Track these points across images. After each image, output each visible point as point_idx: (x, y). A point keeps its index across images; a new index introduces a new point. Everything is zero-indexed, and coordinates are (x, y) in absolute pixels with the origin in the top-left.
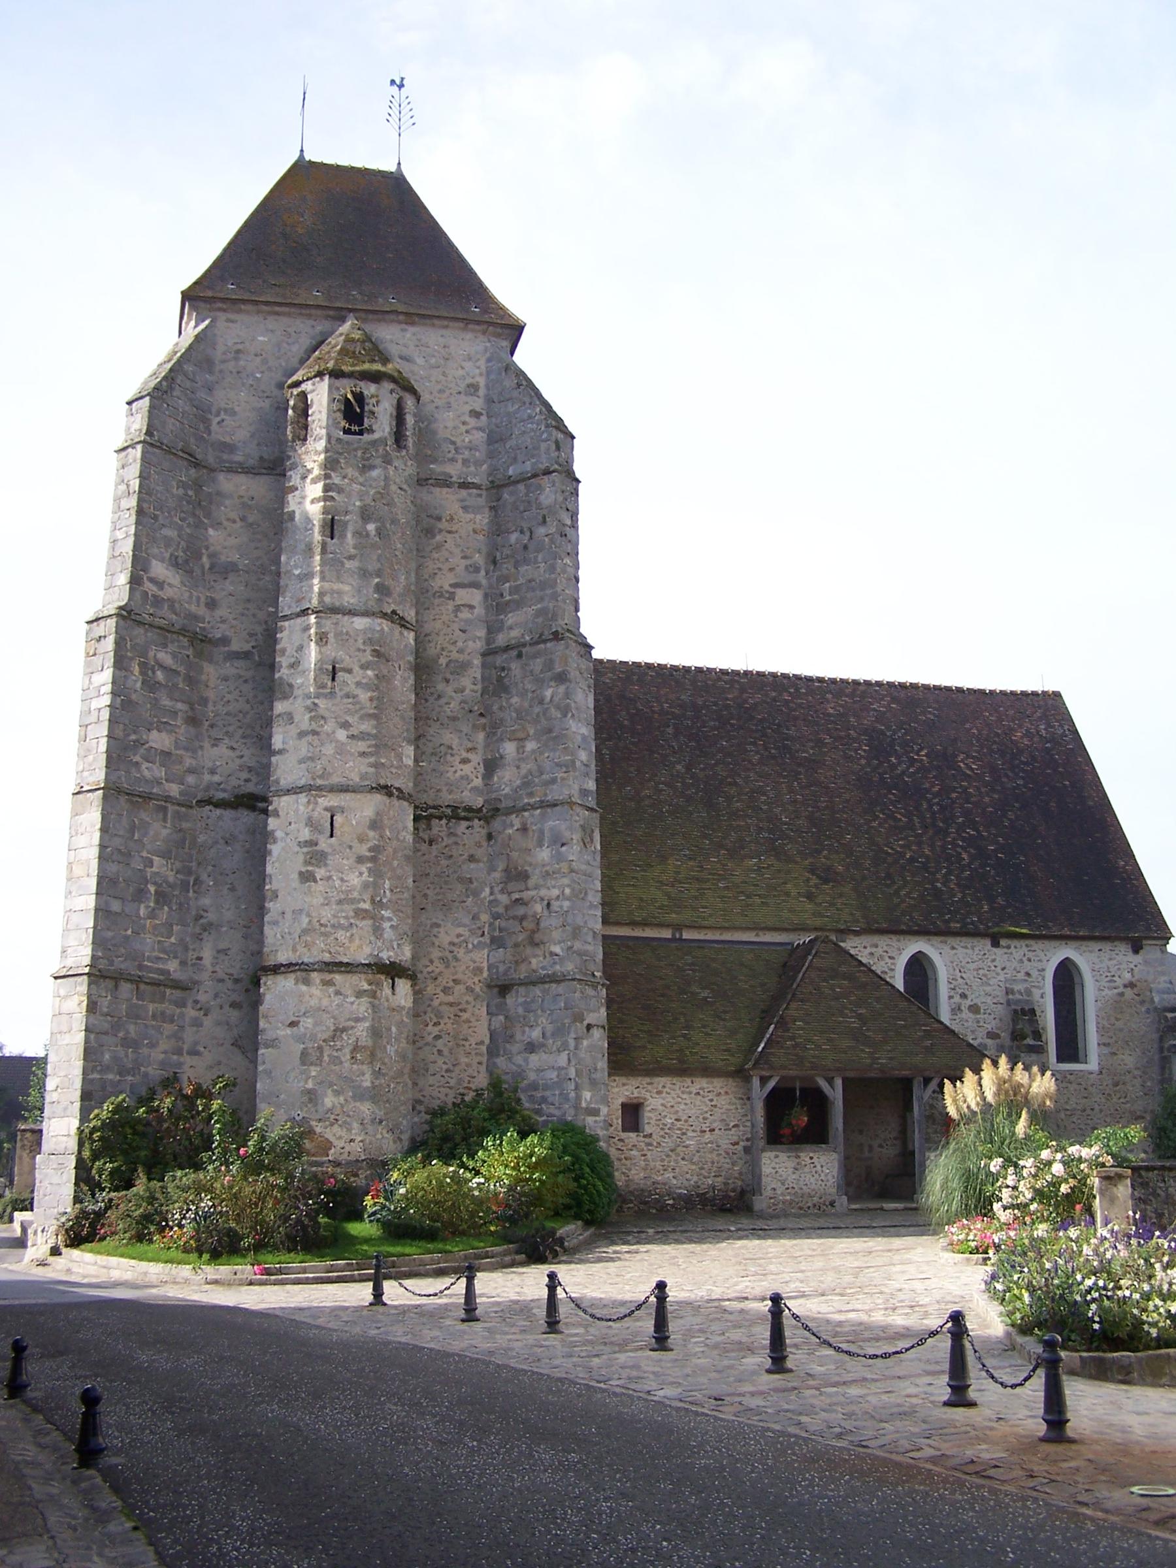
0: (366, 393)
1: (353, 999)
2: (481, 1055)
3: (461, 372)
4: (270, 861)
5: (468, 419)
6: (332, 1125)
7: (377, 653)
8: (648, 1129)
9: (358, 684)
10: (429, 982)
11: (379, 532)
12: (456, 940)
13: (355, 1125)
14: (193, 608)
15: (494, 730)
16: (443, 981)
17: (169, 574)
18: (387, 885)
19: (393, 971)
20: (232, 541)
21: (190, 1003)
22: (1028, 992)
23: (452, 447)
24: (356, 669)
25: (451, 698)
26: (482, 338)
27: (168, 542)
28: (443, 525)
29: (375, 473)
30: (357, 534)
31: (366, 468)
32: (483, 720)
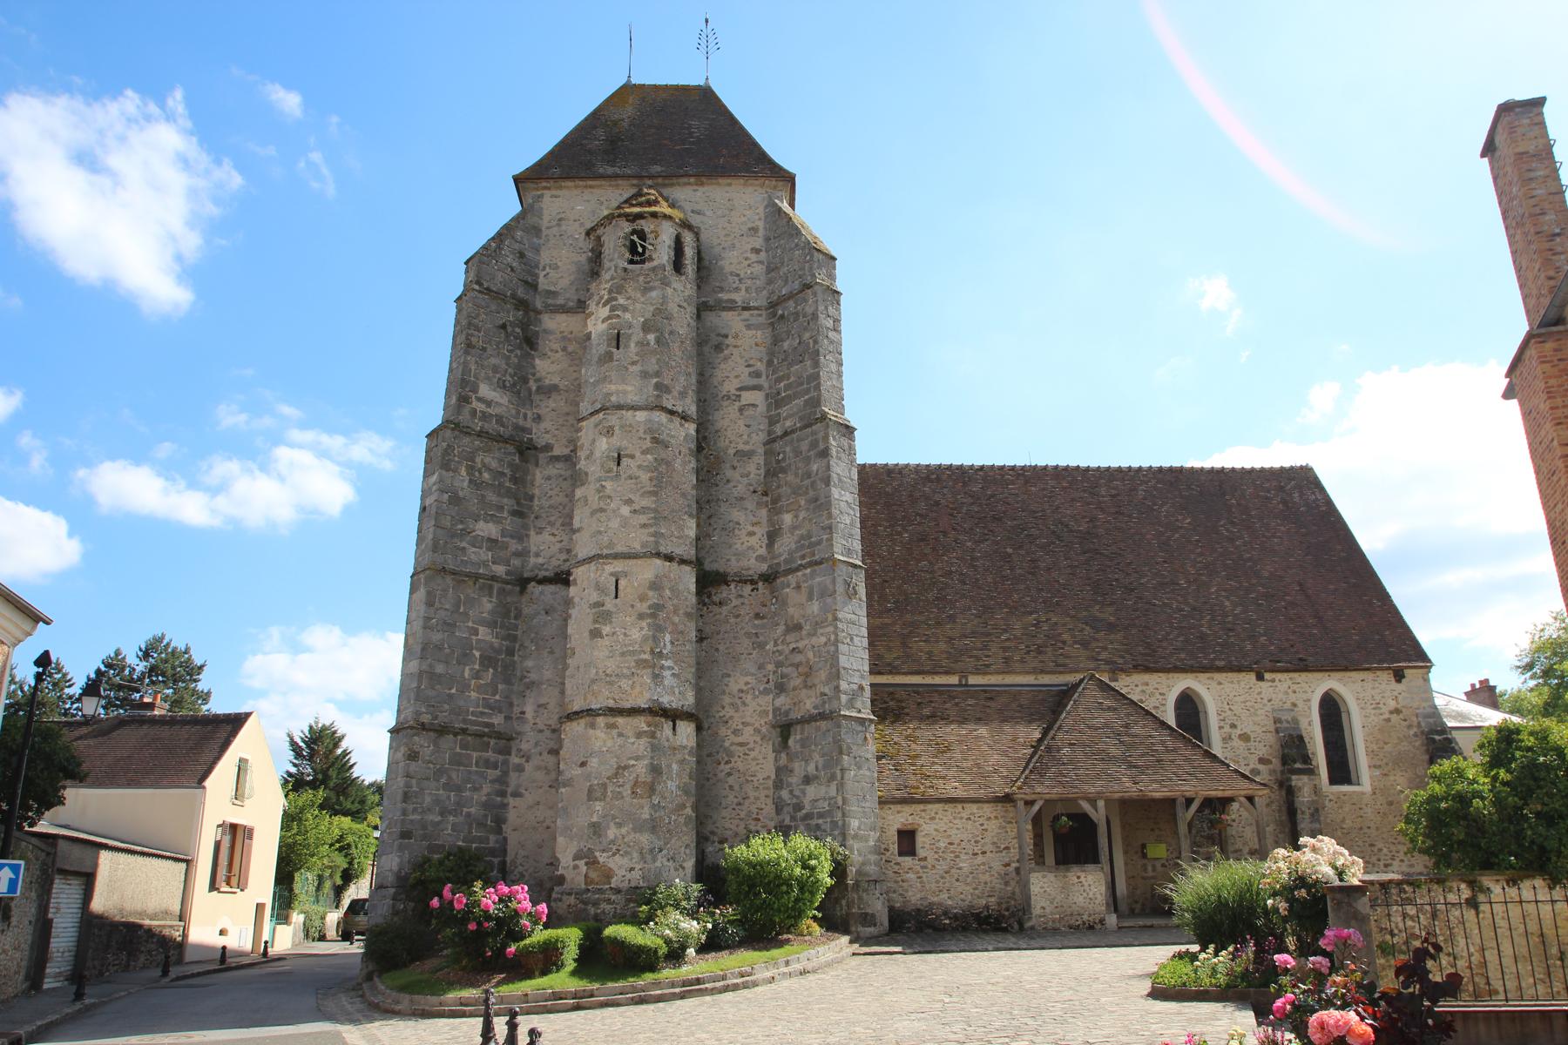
4: (571, 622)
7: (655, 440)
8: (921, 853)
11: (658, 341)
13: (635, 855)
14: (521, 422)
15: (775, 508)
16: (733, 725)
18: (668, 637)
19: (673, 715)
20: (554, 368)
22: (1295, 721)
24: (638, 454)
27: (495, 369)
28: (730, 341)
29: (654, 294)
30: (640, 344)
31: (646, 290)
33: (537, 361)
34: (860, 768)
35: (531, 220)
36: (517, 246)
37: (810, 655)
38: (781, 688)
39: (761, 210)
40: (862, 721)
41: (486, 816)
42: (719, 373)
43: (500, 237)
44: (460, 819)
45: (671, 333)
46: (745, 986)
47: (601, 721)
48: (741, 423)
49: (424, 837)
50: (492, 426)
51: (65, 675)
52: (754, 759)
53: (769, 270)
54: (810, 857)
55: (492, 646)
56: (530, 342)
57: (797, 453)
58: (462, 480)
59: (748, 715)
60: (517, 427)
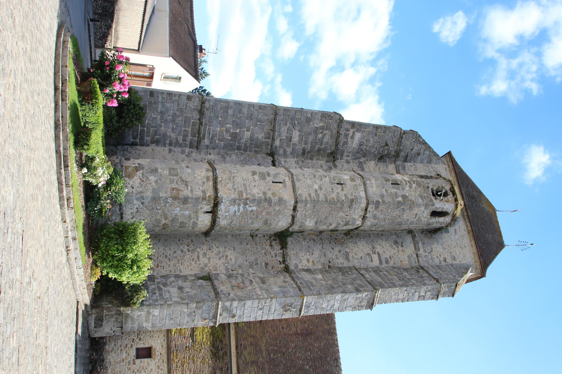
0: (449, 197)
1: (201, 188)
2: (175, 271)
3: (458, 253)
5: (442, 256)
6: (140, 179)
7: (352, 201)
8: (138, 361)
9: (338, 193)
10: (208, 246)
11: (399, 202)
12: (228, 258)
13: (140, 189)
14: (345, 154)
16: (209, 253)
17: (357, 140)
18: (254, 208)
19: (214, 212)
21: (191, 150)
23: (430, 251)
24: (344, 192)
25: (333, 254)
26: (473, 261)
27: (368, 141)
29: (420, 200)
30: (396, 194)
32: (327, 267)
33: (373, 162)
34: (189, 315)
35: (434, 159)
36: (422, 152)
37: (250, 288)
38: (230, 276)
39: (464, 262)
40: (215, 317)
41: (160, 135)
42: (383, 243)
43: (424, 143)
44: (159, 122)
45: (404, 209)
46: (61, 198)
47: (210, 174)
48: (362, 254)
49: (150, 103)
50: (342, 139)
51: (204, 77)
52: (191, 264)
53: (438, 266)
54: (138, 267)
55: (241, 138)
56: (381, 158)
57: (354, 279)
58: (318, 124)
59: (214, 259)
60: (343, 152)
